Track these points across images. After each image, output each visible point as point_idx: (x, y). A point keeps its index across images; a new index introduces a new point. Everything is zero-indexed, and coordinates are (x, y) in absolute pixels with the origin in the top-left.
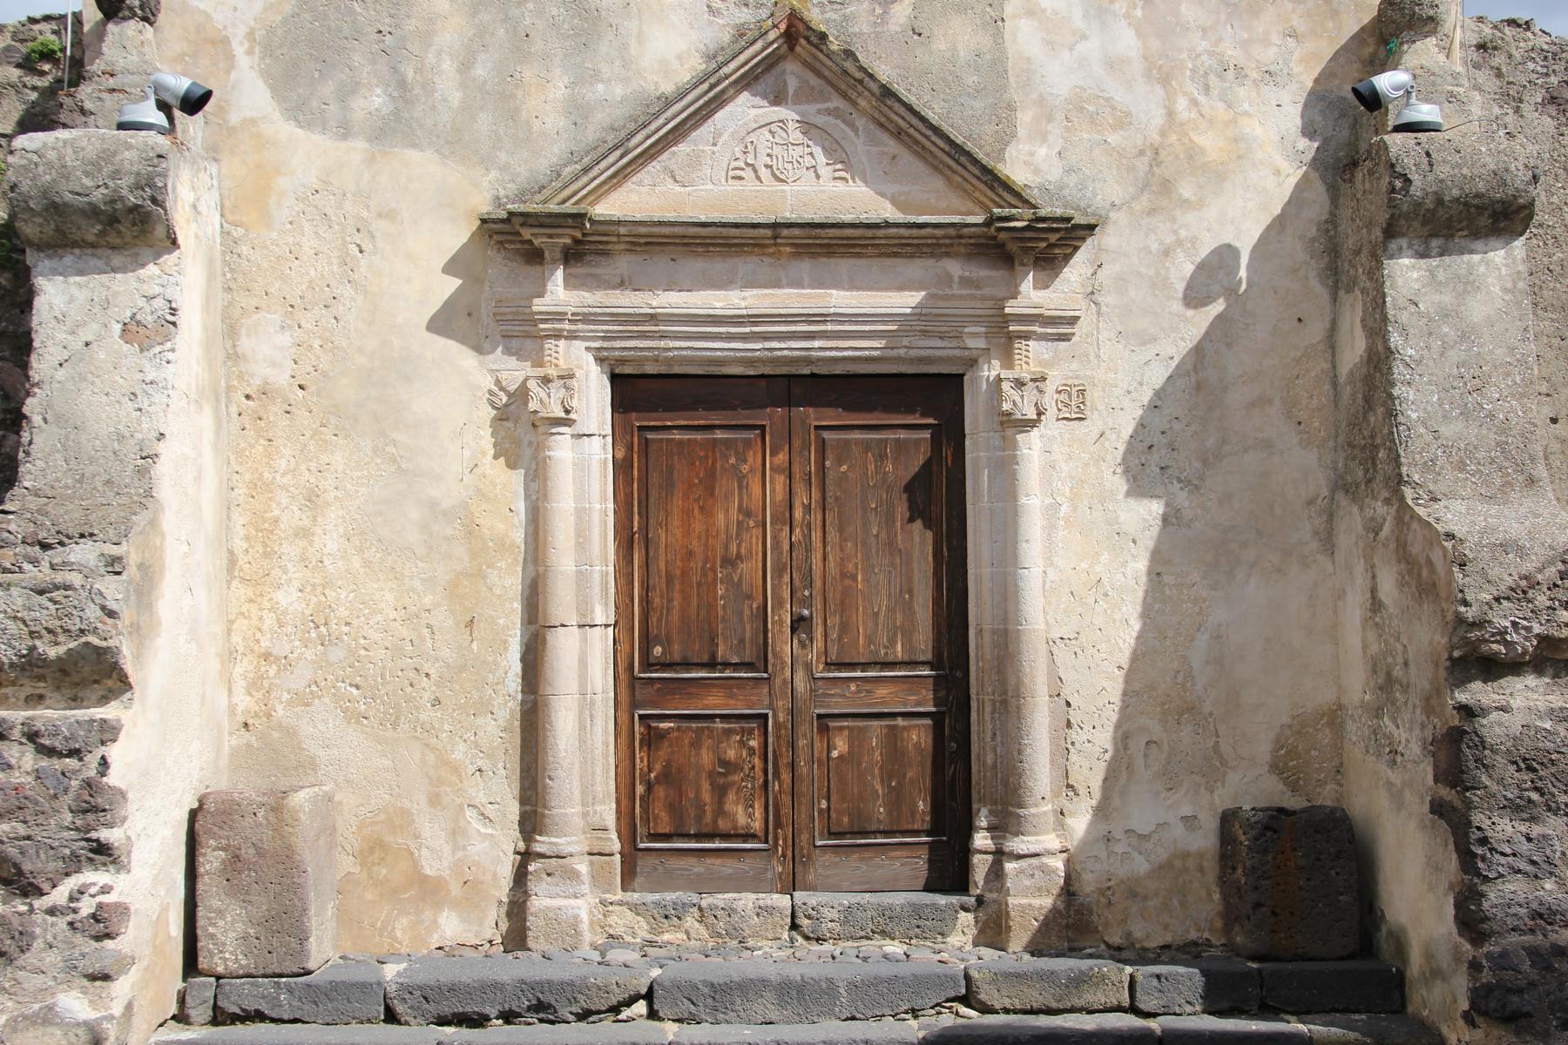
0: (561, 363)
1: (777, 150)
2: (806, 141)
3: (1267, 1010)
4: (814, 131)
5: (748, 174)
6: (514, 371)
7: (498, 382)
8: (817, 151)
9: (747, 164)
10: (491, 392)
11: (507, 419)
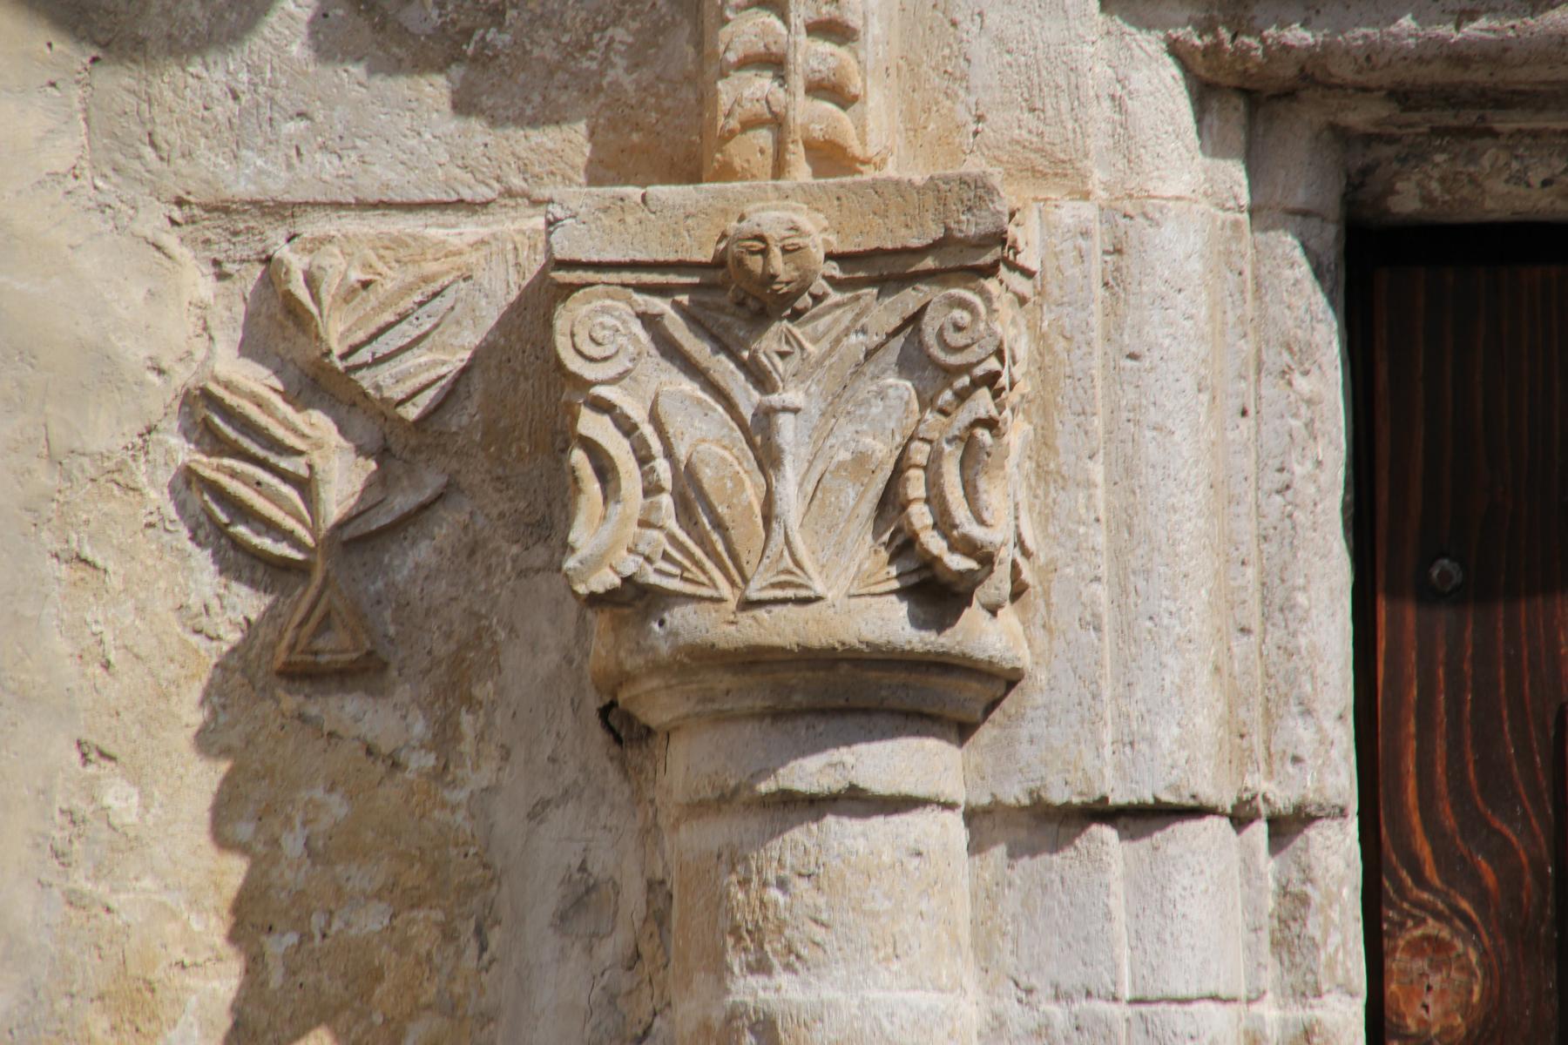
0: (879, 130)
3: (1387, 663)
6: (443, 215)
7: (278, 321)
10: (209, 417)
11: (365, 672)
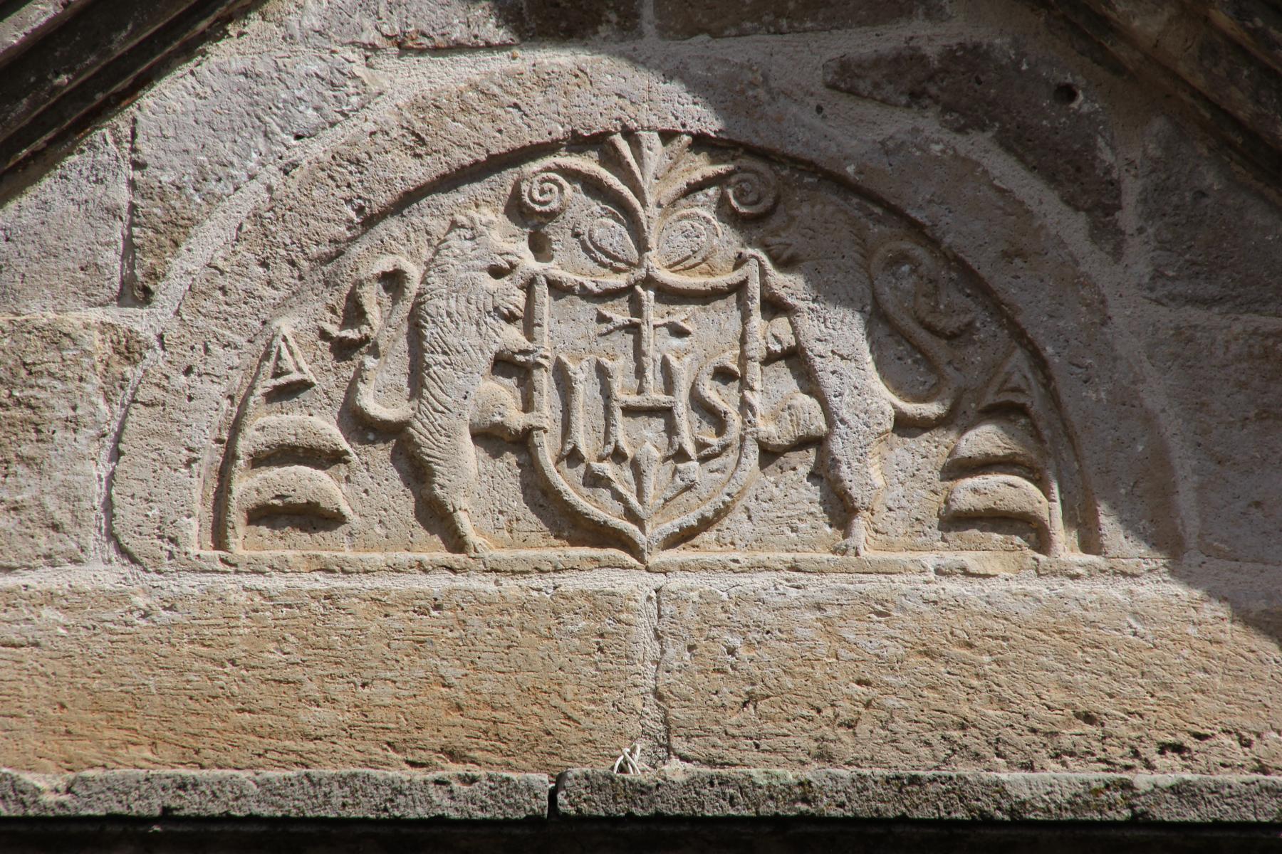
1: (563, 333)
2: (759, 272)
4: (814, 211)
5: (366, 490)
8: (839, 336)
9: (360, 426)
